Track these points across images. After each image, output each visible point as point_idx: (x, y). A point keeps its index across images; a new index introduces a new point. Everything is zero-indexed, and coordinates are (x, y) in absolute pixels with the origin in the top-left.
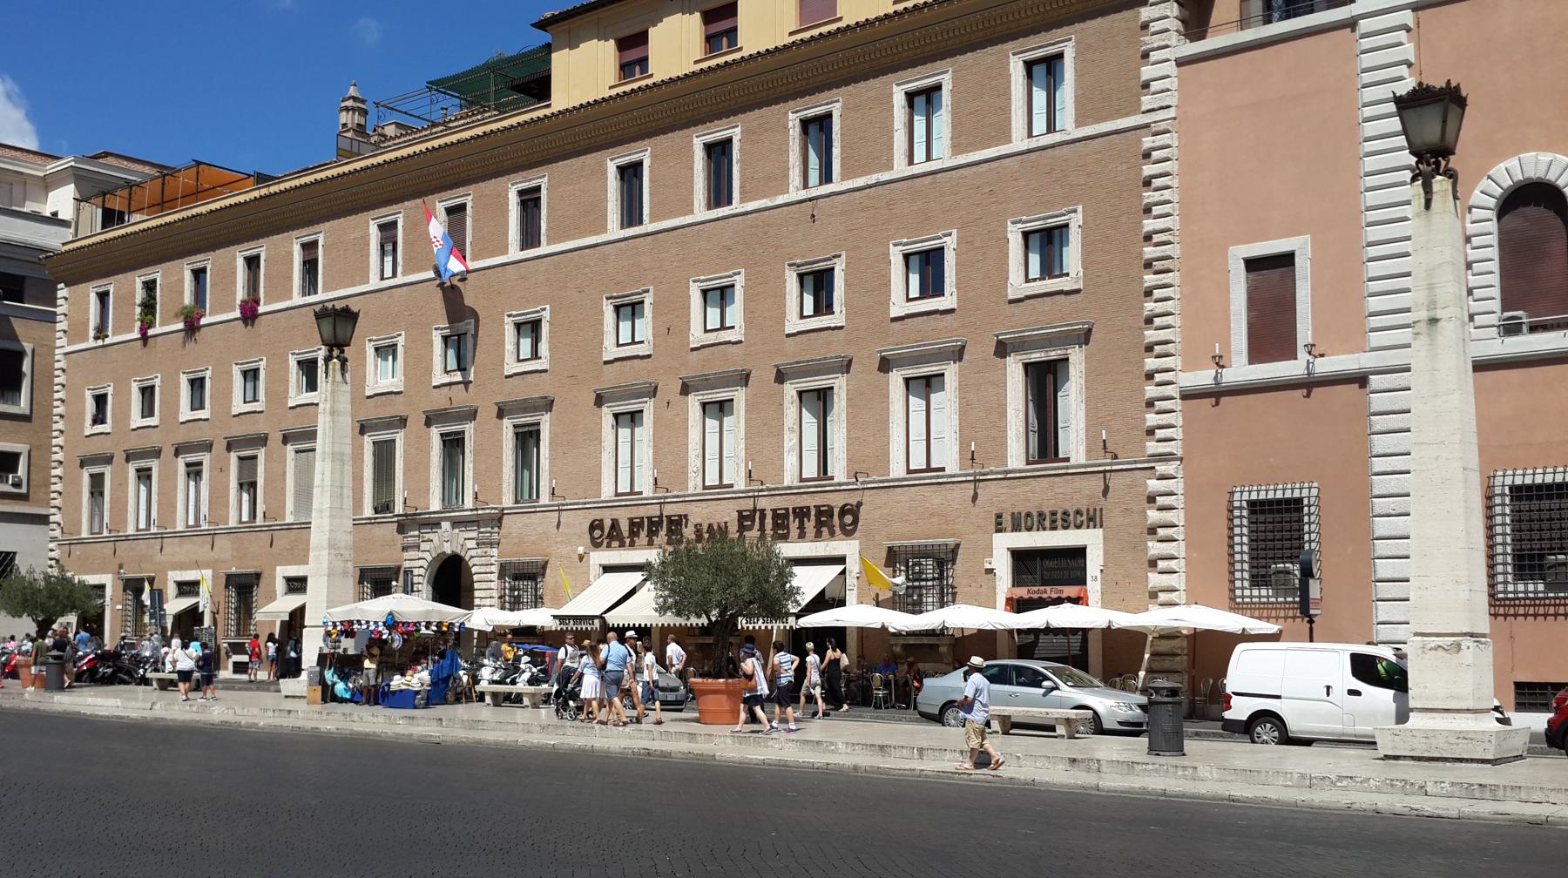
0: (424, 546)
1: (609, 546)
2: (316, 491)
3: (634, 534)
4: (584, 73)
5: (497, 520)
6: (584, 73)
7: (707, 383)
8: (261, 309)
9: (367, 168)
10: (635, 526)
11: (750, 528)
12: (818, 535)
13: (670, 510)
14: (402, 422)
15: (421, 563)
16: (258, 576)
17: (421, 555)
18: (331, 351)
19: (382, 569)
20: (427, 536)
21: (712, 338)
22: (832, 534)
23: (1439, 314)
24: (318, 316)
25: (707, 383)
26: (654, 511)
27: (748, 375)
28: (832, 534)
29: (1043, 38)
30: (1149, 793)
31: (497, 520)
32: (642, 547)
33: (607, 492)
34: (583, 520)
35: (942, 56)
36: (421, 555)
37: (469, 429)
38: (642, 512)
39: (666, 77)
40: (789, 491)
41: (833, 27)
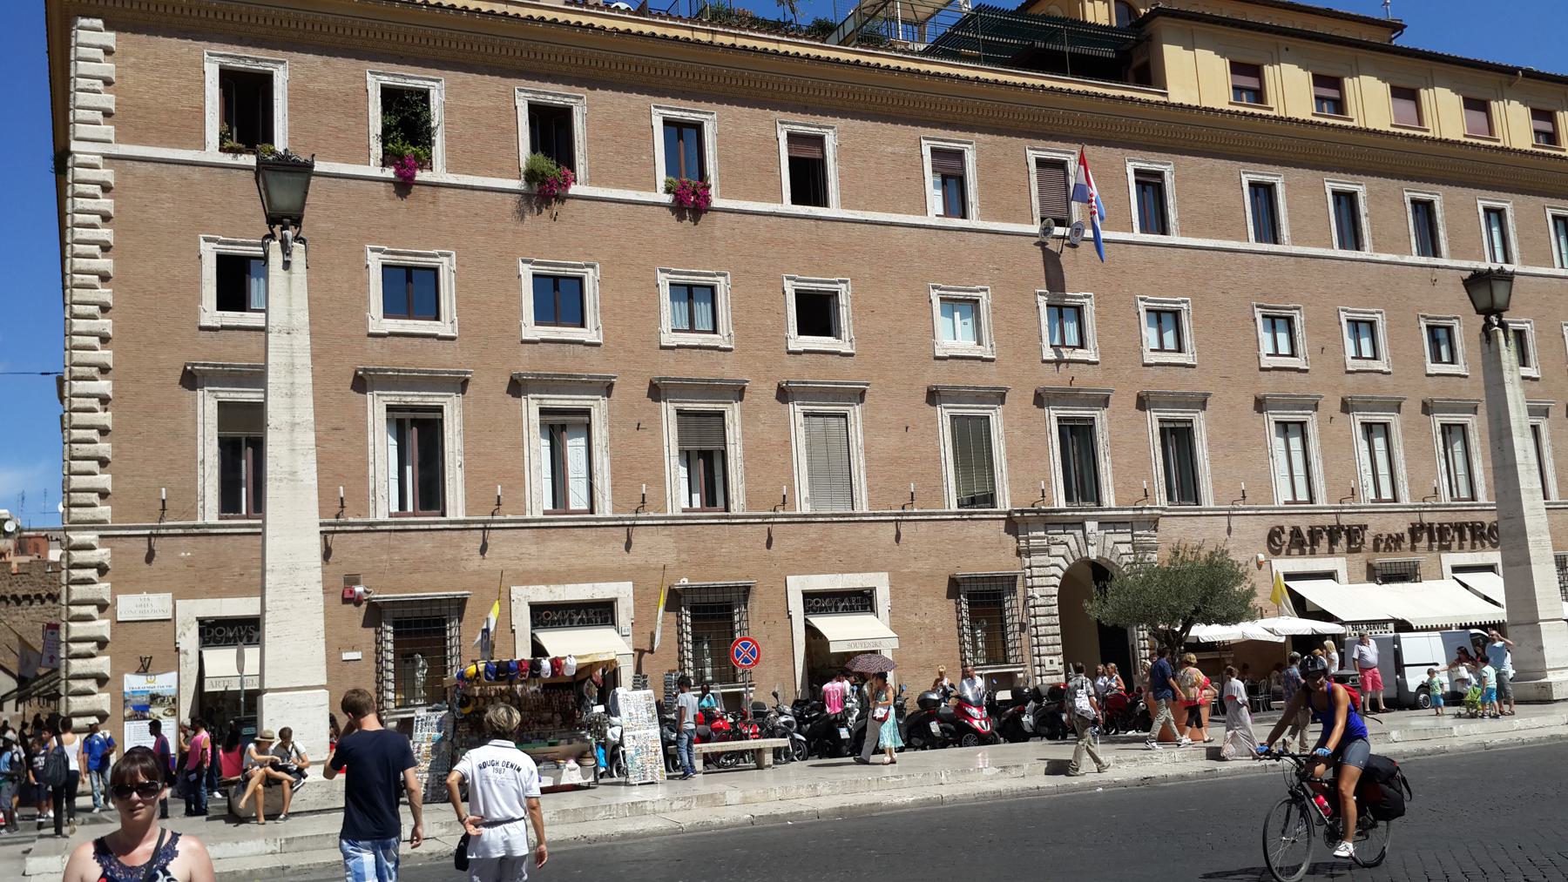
0: (1054, 550)
1: (1288, 554)
2: (1520, 468)
3: (1314, 541)
4: (1195, 76)
5: (1153, 523)
6: (1195, 76)
7: (1369, 405)
8: (574, 190)
9: (938, 74)
10: (1315, 534)
11: (1420, 540)
12: (1473, 547)
13: (1346, 520)
14: (1000, 397)
15: (1054, 570)
16: (746, 591)
17: (1053, 561)
18: (1487, 319)
19: (992, 578)
20: (1060, 538)
21: (1362, 365)
22: (1483, 546)
23: (287, 400)
24: (1466, 283)
25: (1369, 405)
26: (1330, 521)
27: (466, 381)
28: (1483, 546)
29: (1058, 145)
30: (727, 834)
31: (1153, 523)
32: (1323, 555)
33: (1283, 494)
34: (1261, 529)
35: (1366, 173)
36: (1053, 561)
37: (1101, 417)
38: (1318, 521)
39: (1177, 101)
40: (1446, 509)
41: (1419, 133)
